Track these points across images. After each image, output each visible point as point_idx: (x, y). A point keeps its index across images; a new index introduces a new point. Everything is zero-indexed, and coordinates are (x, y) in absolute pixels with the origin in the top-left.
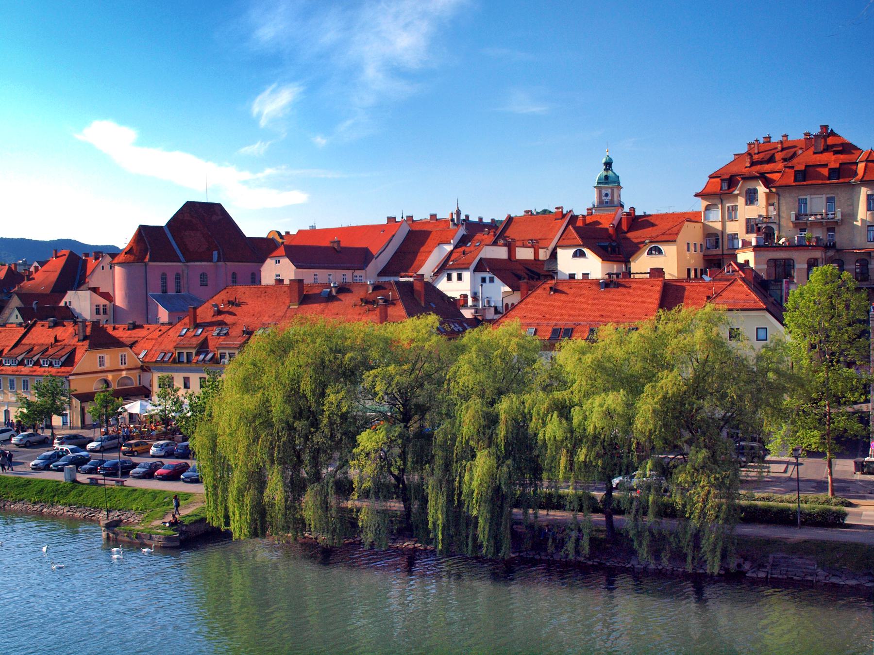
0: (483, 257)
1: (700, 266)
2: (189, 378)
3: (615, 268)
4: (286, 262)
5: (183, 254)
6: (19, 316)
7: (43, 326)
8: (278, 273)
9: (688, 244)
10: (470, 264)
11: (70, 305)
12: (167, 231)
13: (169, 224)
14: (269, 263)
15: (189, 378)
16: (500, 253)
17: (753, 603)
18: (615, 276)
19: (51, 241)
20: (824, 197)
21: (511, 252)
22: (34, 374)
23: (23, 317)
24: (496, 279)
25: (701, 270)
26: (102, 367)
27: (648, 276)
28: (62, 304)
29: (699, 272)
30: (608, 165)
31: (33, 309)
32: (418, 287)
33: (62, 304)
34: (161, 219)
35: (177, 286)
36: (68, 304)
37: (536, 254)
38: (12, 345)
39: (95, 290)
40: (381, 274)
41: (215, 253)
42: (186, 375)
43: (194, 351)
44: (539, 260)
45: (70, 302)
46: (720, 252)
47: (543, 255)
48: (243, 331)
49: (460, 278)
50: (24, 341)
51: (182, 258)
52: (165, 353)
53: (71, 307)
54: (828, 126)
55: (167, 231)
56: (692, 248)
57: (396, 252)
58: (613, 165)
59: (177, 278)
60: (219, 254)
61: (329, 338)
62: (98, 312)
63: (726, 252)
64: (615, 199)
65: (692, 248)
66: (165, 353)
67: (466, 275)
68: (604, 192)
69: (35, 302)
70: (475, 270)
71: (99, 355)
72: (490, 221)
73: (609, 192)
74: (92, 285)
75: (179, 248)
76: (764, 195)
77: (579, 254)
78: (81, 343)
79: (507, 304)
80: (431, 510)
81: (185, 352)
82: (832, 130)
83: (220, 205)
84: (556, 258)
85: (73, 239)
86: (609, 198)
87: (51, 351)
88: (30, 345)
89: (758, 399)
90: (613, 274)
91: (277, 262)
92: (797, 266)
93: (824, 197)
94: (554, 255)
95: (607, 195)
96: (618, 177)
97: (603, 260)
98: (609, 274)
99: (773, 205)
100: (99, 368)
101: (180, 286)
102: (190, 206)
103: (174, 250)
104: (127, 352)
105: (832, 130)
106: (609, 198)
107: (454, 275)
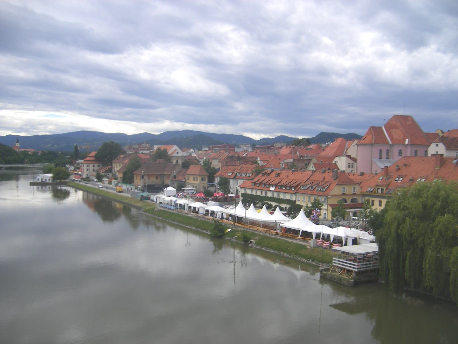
4: (441, 145)
6: (314, 167)
7: (320, 172)
8: (437, 151)
11: (337, 163)
14: (433, 145)
17: (319, 282)
19: (345, 134)
22: (313, 194)
28: (334, 162)
33: (334, 162)
35: (380, 156)
36: (336, 162)
39: (349, 156)
42: (381, 199)
43: (385, 188)
45: (337, 161)
48: (410, 180)
50: (311, 178)
53: (337, 164)
59: (387, 152)
60: (408, 140)
61: (438, 186)
62: (349, 167)
74: (348, 154)
75: (389, 137)
78: (334, 181)
80: (241, 230)
85: (355, 133)
87: (321, 184)
88: (313, 180)
89: (286, 187)
91: (437, 145)
101: (388, 156)
103: (386, 139)
104: (357, 187)
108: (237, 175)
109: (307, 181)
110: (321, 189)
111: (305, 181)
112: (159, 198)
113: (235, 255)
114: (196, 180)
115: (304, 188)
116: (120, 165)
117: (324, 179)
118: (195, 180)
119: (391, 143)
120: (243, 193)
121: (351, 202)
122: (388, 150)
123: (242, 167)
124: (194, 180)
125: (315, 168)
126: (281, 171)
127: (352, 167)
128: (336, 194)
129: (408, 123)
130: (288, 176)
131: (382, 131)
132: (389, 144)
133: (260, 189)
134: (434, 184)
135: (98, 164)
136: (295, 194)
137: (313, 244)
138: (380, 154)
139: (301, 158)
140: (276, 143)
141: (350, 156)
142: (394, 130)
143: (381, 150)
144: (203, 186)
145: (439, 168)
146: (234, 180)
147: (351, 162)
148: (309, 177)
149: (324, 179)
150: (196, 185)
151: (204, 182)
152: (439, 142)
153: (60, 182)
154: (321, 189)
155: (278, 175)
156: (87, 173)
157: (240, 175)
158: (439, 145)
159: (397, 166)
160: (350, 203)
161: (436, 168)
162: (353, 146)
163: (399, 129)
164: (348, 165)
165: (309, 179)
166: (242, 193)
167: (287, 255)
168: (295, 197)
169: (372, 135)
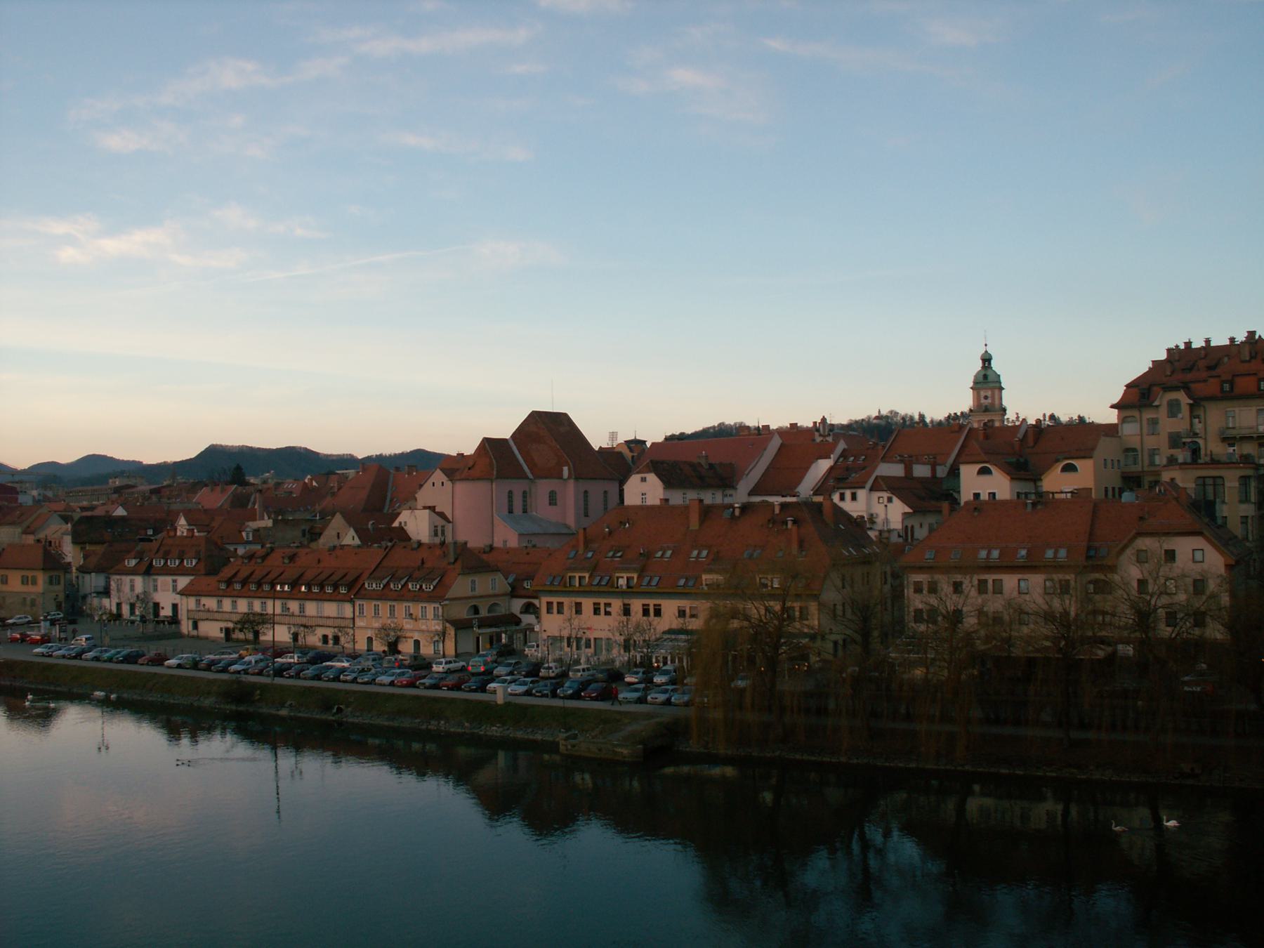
0: (879, 474)
1: (1118, 483)
2: (581, 603)
3: (1026, 487)
4: (652, 478)
5: (531, 470)
6: (356, 537)
7: (405, 547)
9: (1105, 460)
10: (865, 482)
11: (406, 525)
12: (512, 443)
13: (519, 434)
15: (581, 603)
16: (896, 470)
18: (1023, 496)
20: (1254, 409)
21: (908, 469)
23: (360, 538)
24: (895, 499)
25: (1120, 489)
26: (473, 593)
27: (1069, 495)
28: (396, 524)
29: (1117, 491)
30: (987, 360)
31: (368, 529)
32: (827, 508)
33: (396, 524)
34: (505, 429)
36: (403, 524)
37: (934, 471)
38: (373, 567)
40: (751, 493)
41: (566, 469)
44: (913, 479)
45: (405, 523)
46: (1140, 469)
47: (942, 472)
49: (854, 497)
51: (530, 476)
52: (554, 577)
53: (405, 528)
54: (1255, 332)
55: (512, 443)
56: (1109, 465)
57: (768, 468)
58: (992, 362)
60: (569, 469)
62: (436, 535)
63: (1146, 469)
64: (997, 402)
65: (1109, 465)
66: (554, 577)
67: (862, 494)
68: (983, 394)
69: (371, 522)
70: (871, 490)
71: (470, 579)
72: (811, 425)
73: (989, 393)
76: (1188, 407)
77: (984, 471)
78: (452, 566)
79: (907, 527)
81: (577, 575)
82: (1260, 336)
83: (565, 415)
84: (958, 475)
86: (989, 401)
90: (1022, 493)
91: (644, 480)
92: (1227, 484)
93: (1254, 409)
94: (954, 472)
95: (986, 398)
96: (999, 376)
97: (1012, 479)
98: (1019, 494)
99: (1198, 417)
100: (470, 594)
102: (536, 417)
105: (1260, 336)
106: (989, 401)
107: (848, 494)
108: (154, 564)
110: (421, 586)
111: (371, 571)
112: (189, 614)
113: (274, 756)
114: (32, 584)
115: (374, 586)
118: (27, 584)
119: (530, 476)
121: (489, 612)
122: (525, 492)
123: (163, 543)
124: (25, 581)
126: (297, 550)
127: (443, 533)
128: (459, 595)
130: (319, 561)
131: (510, 448)
132: (527, 478)
134: (693, 559)
136: (351, 601)
137: (502, 697)
138: (509, 501)
139: (280, 518)
140: (115, 478)
141: (435, 509)
143: (510, 492)
144: (55, 599)
145: (1093, 496)
146: (146, 577)
147: (440, 522)
148: (379, 561)
149: (423, 563)
150: (33, 597)
151: (57, 588)
152: (647, 472)
154: (421, 586)
155: (292, 558)
156: (1113, 486)
157: (177, 564)
158: (647, 479)
160: (487, 615)
162: (432, 484)
164: (433, 529)
165: (380, 565)
166: (109, 597)
168: (352, 609)
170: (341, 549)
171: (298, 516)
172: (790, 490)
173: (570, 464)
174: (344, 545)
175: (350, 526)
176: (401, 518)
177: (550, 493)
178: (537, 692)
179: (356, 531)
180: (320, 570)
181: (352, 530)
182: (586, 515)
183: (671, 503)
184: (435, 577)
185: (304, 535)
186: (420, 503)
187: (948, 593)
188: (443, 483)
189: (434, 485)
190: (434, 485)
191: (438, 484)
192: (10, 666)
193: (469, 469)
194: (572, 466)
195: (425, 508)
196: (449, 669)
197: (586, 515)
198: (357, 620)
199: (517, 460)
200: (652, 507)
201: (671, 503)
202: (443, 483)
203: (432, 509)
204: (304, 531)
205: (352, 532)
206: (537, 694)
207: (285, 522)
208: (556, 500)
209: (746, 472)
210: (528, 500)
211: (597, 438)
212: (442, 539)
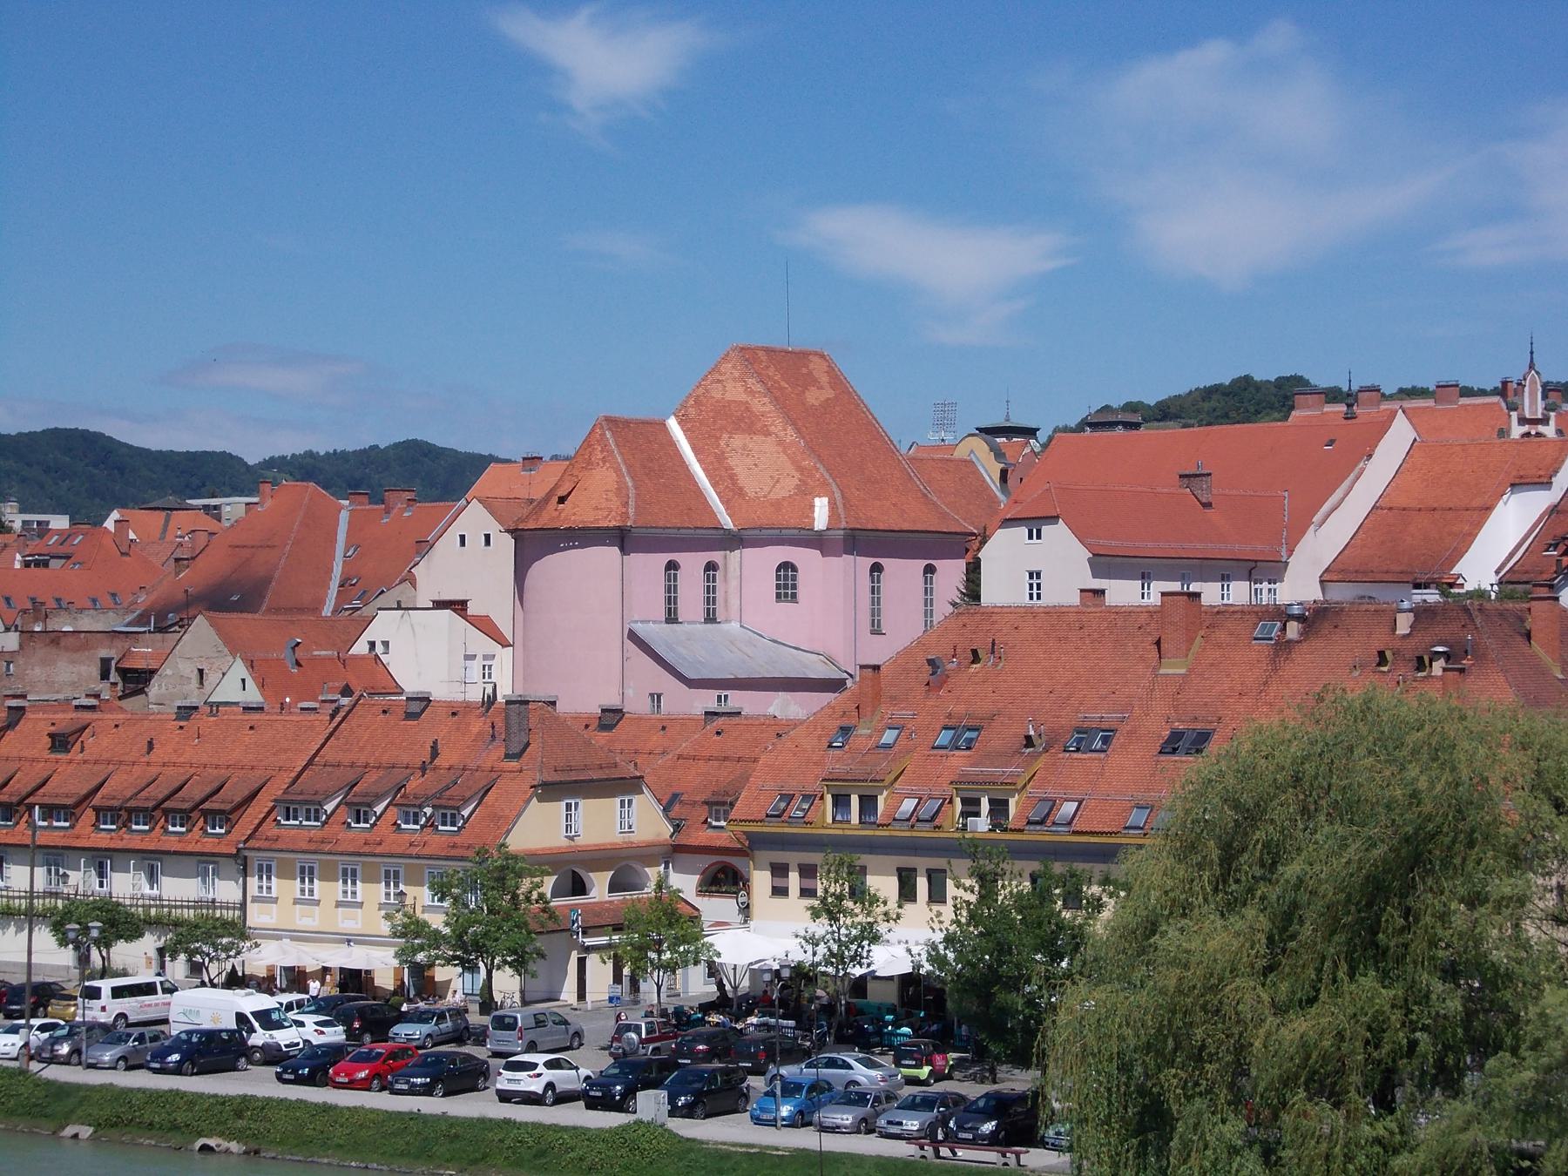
6: (250, 683)
33: (361, 648)
36: (379, 649)
45: (386, 644)
50: (329, 754)
60: (832, 506)
75: (714, 485)
78: (514, 764)
109: (177, 784)
111: (293, 775)
116: (1146, 585)
117: (435, 752)
120: (797, 874)
125: (262, 686)
129: (814, 397)
133: (189, 848)
135: (874, 560)
142: (738, 441)
149: (435, 752)
153: (703, 1018)
159: (928, 660)
161: (1162, 671)
163: (768, 434)
167: (1472, 1139)
169: (618, 471)
170: (211, 714)
171: (87, 623)
172: (1267, 568)
173: (835, 489)
174: (219, 704)
175: (233, 654)
176: (374, 632)
177: (778, 569)
178: (889, 1123)
179: (251, 665)
180: (154, 771)
181: (239, 662)
182: (876, 631)
183: (1111, 599)
184: (468, 794)
185: (105, 675)
186: (424, 597)
187: (1483, 864)
188: (487, 537)
189: (463, 543)
190: (463, 543)
191: (478, 540)
192: (1200, 1173)
193: (562, 500)
194: (838, 495)
195: (440, 605)
196: (122, 1016)
197: (876, 631)
198: (252, 908)
199: (690, 477)
200: (1057, 613)
201: (1111, 599)
202: (487, 537)
203: (459, 606)
204: (105, 665)
205: (239, 670)
206: (963, 1135)
207: (55, 638)
208: (794, 587)
209: (1317, 518)
210: (719, 595)
211: (252, 460)
212: (489, 690)
